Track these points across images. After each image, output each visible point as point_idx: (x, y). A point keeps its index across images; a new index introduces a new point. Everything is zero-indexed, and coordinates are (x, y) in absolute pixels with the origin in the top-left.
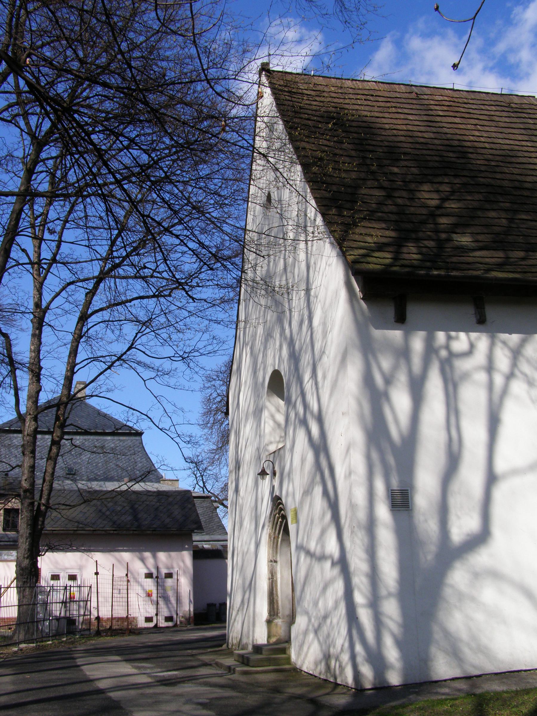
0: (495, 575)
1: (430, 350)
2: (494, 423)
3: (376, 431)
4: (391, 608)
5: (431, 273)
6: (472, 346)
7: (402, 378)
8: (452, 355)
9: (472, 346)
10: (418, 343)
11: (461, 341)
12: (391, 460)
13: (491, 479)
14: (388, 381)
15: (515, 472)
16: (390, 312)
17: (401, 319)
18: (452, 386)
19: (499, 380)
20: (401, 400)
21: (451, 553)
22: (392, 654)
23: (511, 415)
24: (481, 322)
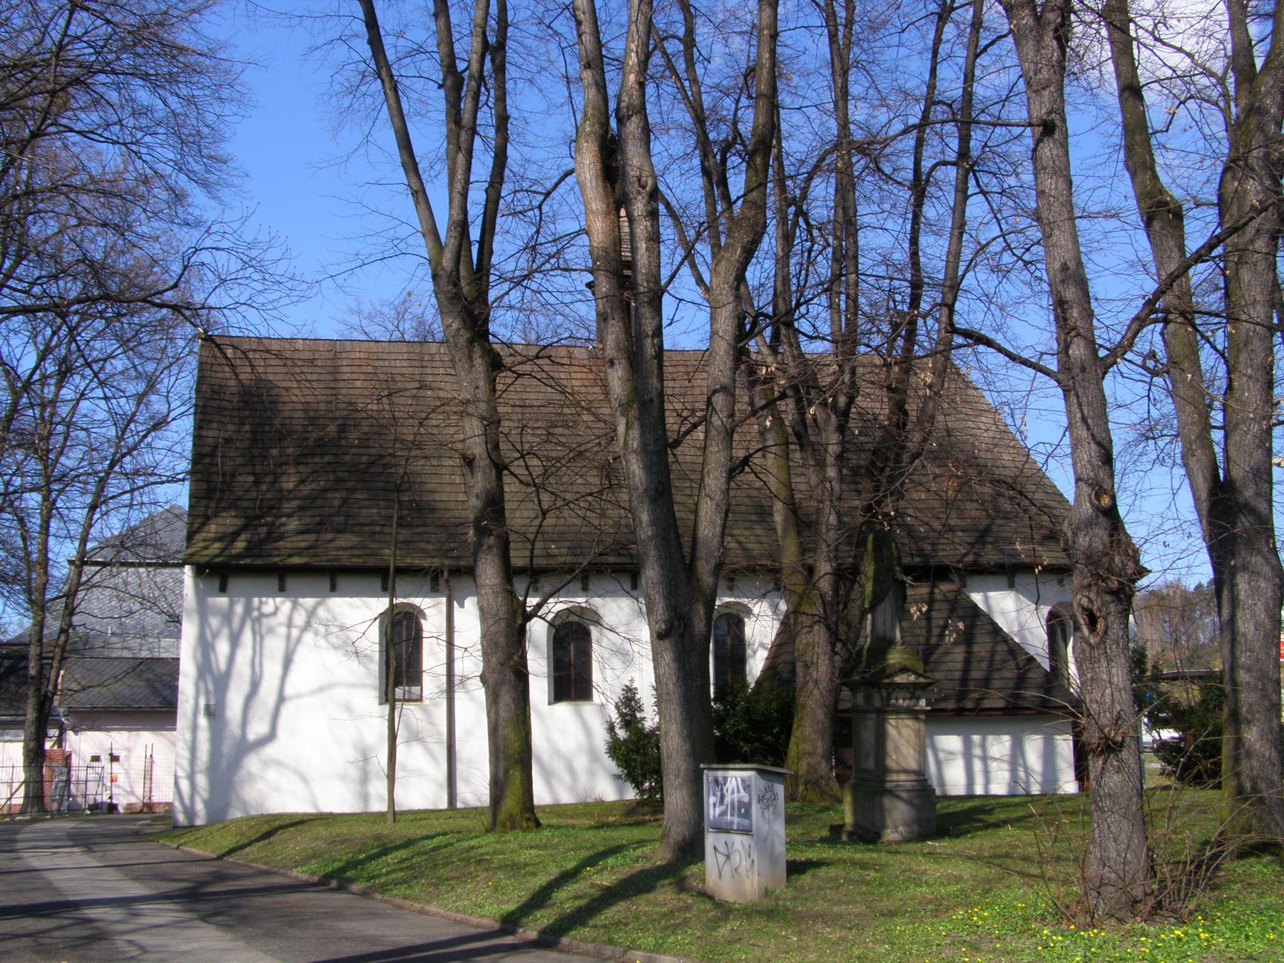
0: (279, 764)
1: (248, 610)
2: (288, 662)
3: (204, 666)
4: (202, 780)
5: (752, 686)
6: (277, 609)
7: (225, 632)
8: (262, 615)
9: (277, 609)
10: (239, 609)
11: (269, 604)
12: (211, 687)
13: (281, 699)
14: (215, 636)
15: (299, 696)
16: (216, 583)
17: (223, 589)
18: (259, 637)
19: (295, 632)
20: (223, 647)
21: (245, 747)
22: (200, 806)
23: (301, 655)
24: (282, 589)
